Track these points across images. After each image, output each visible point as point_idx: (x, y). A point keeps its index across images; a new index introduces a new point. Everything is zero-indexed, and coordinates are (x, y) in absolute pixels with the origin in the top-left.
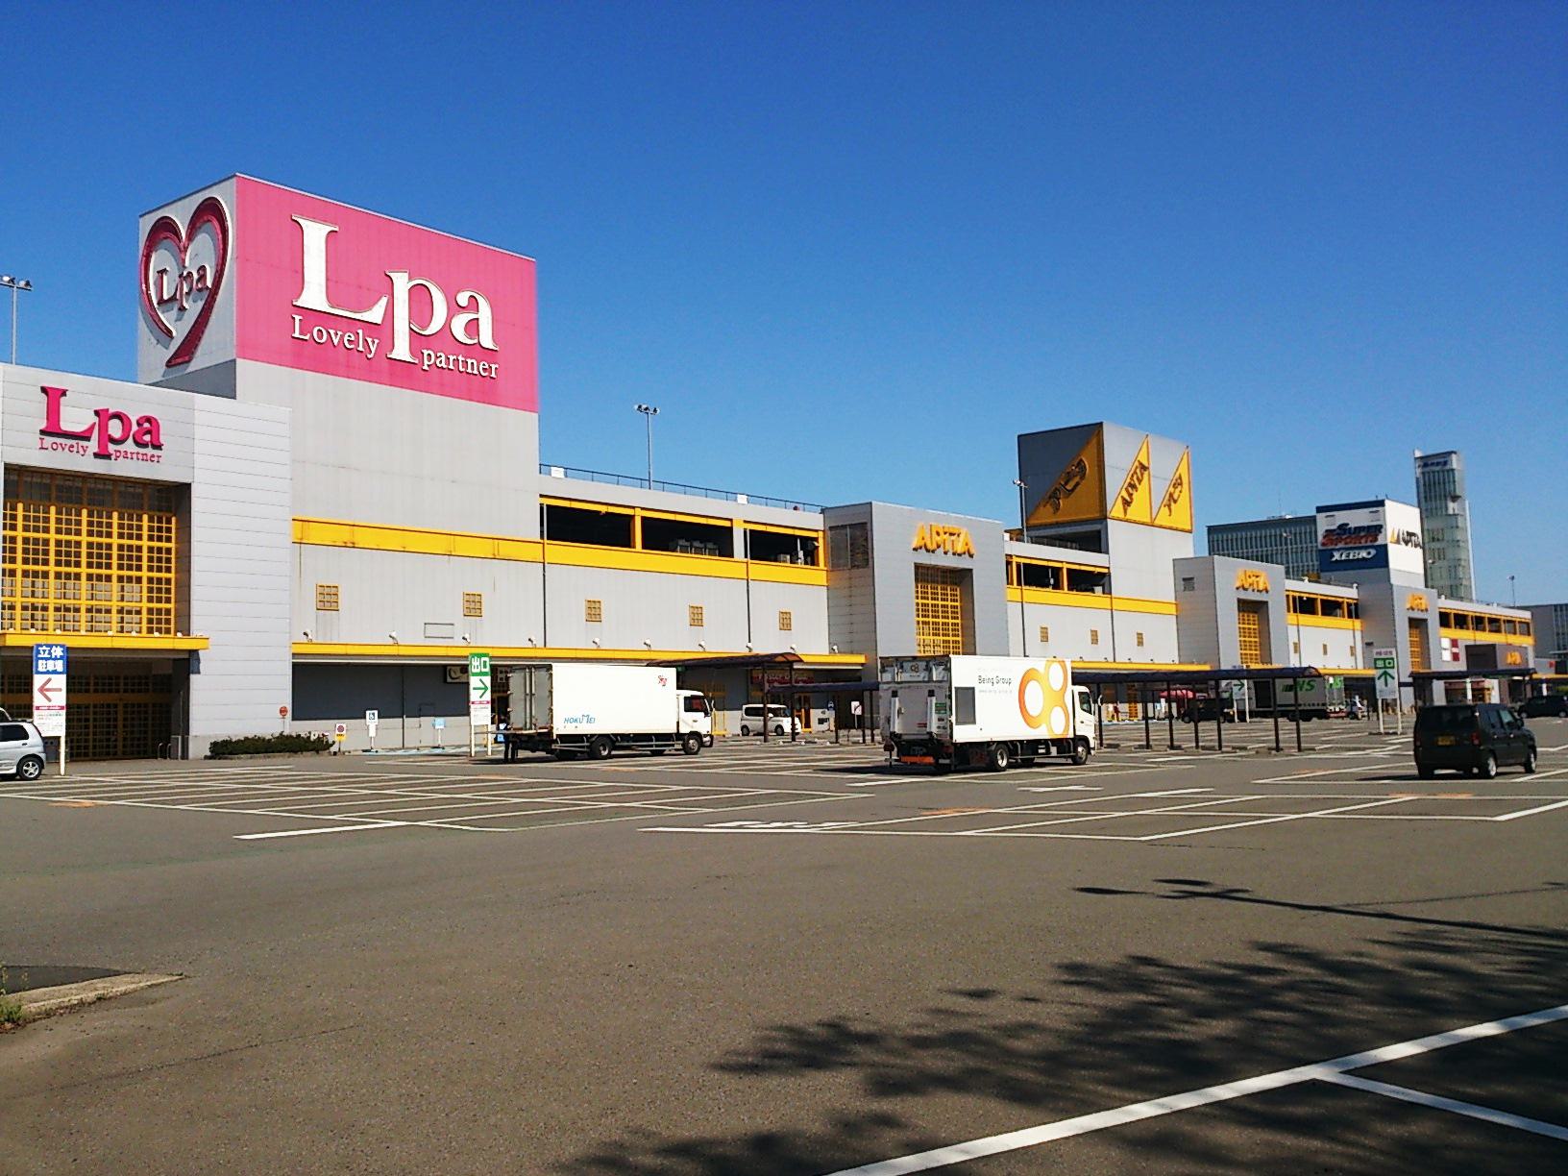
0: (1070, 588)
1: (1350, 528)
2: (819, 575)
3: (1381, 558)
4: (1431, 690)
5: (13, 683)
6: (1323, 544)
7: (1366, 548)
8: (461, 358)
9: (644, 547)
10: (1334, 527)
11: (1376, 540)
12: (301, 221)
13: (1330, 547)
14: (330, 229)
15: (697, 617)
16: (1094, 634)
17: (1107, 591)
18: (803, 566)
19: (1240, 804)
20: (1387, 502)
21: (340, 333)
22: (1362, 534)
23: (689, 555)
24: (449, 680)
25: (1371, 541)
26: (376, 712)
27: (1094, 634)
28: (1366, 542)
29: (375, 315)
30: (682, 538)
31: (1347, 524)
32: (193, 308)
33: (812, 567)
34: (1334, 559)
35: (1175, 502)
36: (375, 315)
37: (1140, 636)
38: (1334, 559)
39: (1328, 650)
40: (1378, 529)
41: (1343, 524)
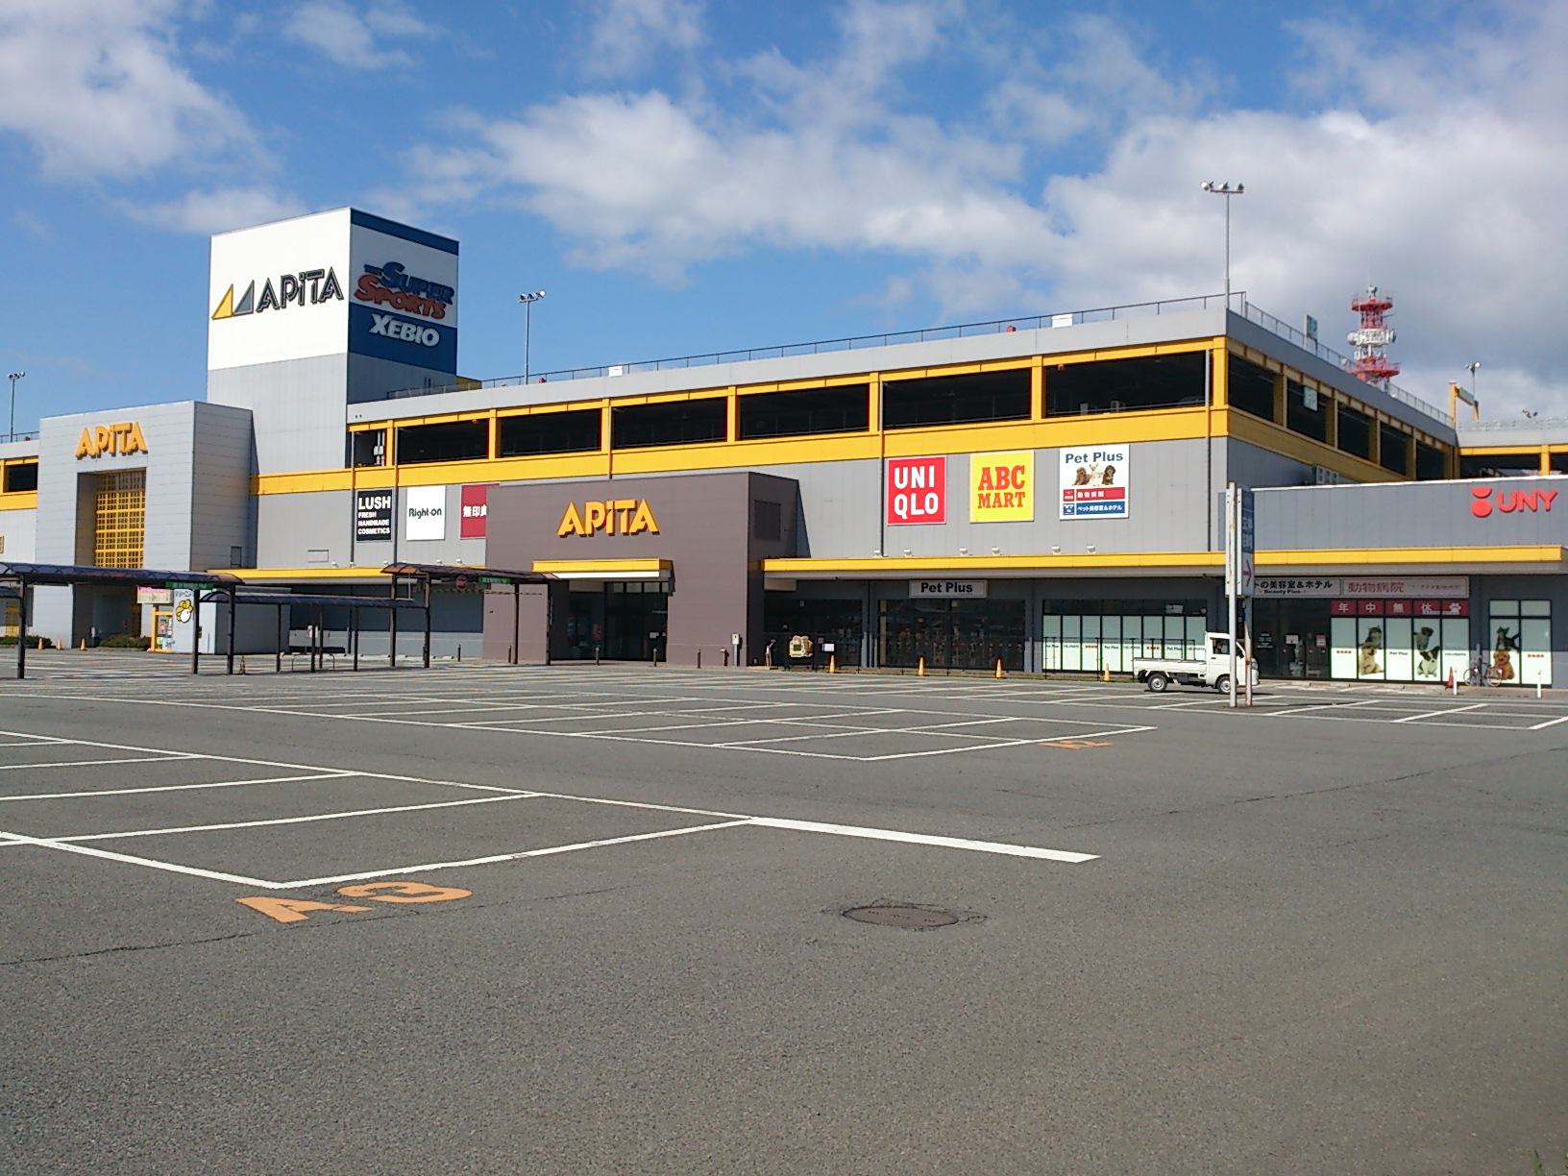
7: (426, 325)
13: (370, 304)
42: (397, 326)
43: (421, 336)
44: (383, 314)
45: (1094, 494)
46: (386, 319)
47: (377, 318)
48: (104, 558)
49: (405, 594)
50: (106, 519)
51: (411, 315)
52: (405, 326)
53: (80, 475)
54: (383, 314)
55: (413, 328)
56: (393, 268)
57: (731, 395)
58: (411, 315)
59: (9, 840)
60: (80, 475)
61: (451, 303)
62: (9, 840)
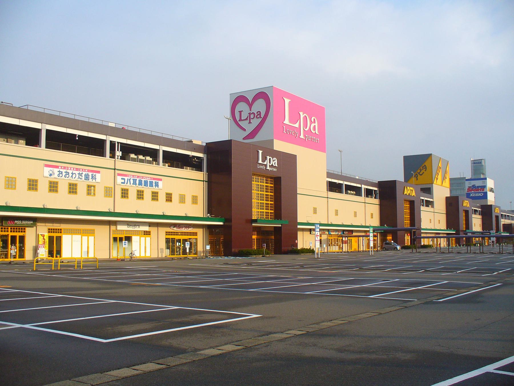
0: (48, 146)
1: (476, 186)
2: (201, 175)
3: (485, 194)
4: (108, 225)
5: (195, 234)
6: (467, 191)
7: (480, 193)
8: (312, 137)
9: (47, 147)
10: (471, 186)
11: (484, 190)
12: (285, 99)
13: (470, 192)
14: (290, 101)
15: (315, 211)
16: (355, 213)
17: (433, 207)
18: (189, 171)
19: (445, 276)
20: (487, 178)
21: (291, 131)
22: (479, 188)
23: (136, 163)
24: (312, 233)
25: (482, 191)
26: (186, 243)
27: (355, 213)
28: (480, 191)
29: (297, 125)
30: (132, 153)
31: (475, 185)
32: (256, 122)
33: (7, 143)
34: (471, 196)
35: (446, 178)
36: (297, 125)
37: (355, 213)
38: (471, 196)
39: (438, 221)
40: (485, 187)
41: (474, 185)
42: (122, 179)
43: (480, 195)
44: (472, 193)
45: (149, 178)
46: (473, 194)
47: (471, 194)
48: (269, 214)
49: (169, 239)
50: (268, 205)
51: (478, 192)
52: (476, 194)
53: (46, 148)
54: (472, 193)
55: (478, 194)
56: (473, 186)
57: (28, 186)
58: (478, 192)
59: (14, 326)
60: (46, 148)
61: (485, 188)
62: (14, 326)
